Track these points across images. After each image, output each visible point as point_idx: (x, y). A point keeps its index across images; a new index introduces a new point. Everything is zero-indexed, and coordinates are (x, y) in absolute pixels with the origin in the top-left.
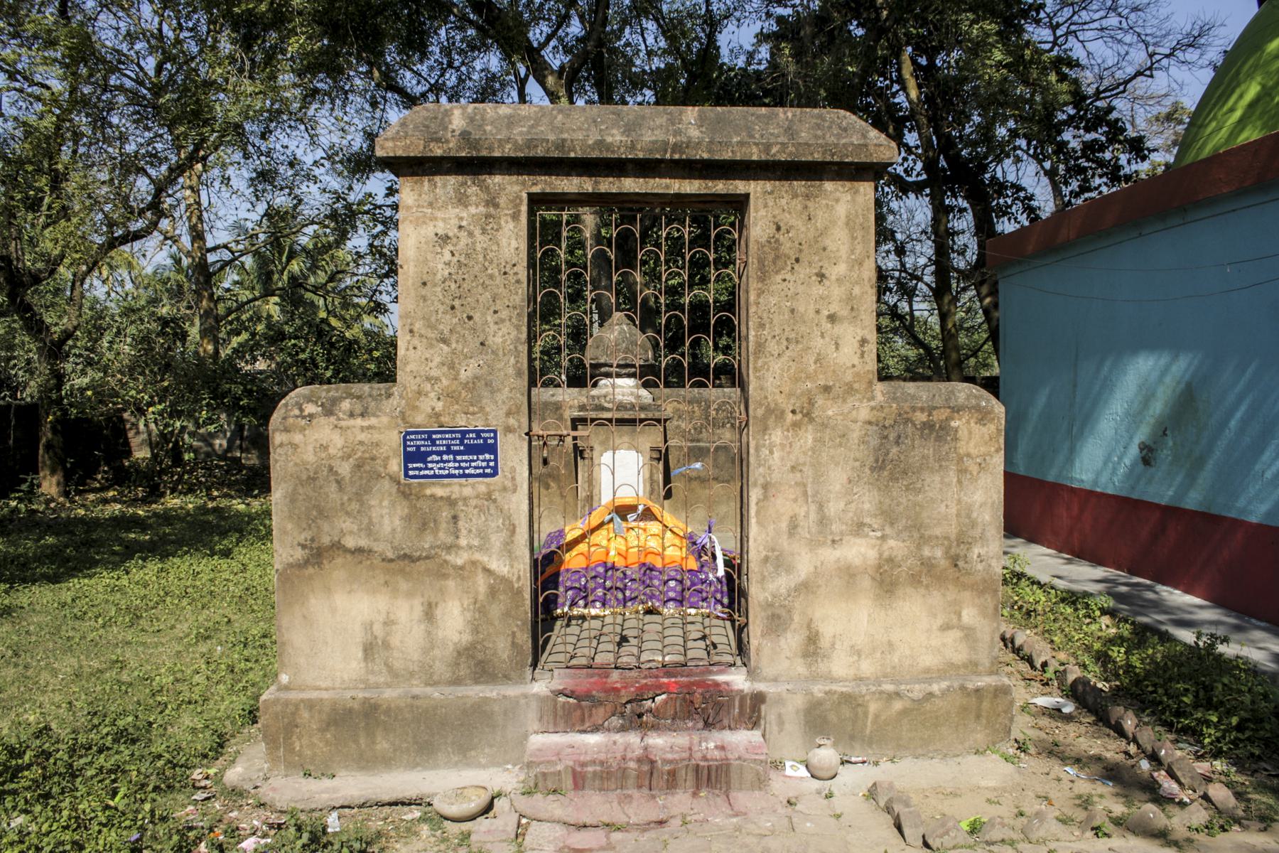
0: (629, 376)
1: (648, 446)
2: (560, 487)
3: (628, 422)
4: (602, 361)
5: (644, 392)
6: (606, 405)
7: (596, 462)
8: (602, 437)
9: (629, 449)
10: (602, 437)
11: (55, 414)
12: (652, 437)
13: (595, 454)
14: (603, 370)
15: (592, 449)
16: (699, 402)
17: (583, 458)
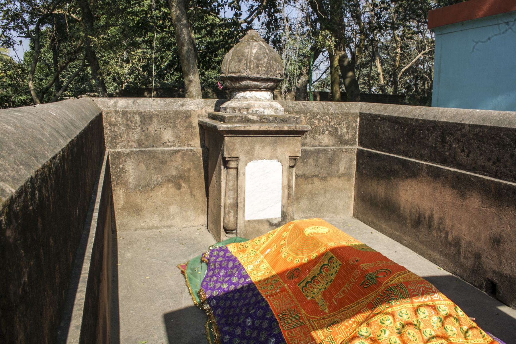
0: (267, 89)
1: (287, 155)
2: (190, 187)
3: (275, 133)
4: (245, 75)
5: (277, 104)
6: (250, 117)
7: (241, 171)
8: (247, 148)
9: (271, 158)
10: (247, 148)
11: (97, 24)
12: (292, 147)
13: (241, 163)
14: (244, 83)
15: (237, 159)
16: (305, 113)
17: (227, 167)
